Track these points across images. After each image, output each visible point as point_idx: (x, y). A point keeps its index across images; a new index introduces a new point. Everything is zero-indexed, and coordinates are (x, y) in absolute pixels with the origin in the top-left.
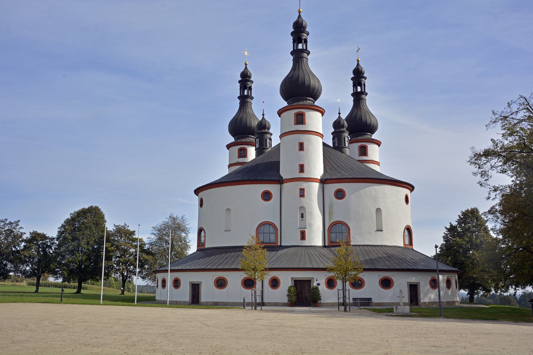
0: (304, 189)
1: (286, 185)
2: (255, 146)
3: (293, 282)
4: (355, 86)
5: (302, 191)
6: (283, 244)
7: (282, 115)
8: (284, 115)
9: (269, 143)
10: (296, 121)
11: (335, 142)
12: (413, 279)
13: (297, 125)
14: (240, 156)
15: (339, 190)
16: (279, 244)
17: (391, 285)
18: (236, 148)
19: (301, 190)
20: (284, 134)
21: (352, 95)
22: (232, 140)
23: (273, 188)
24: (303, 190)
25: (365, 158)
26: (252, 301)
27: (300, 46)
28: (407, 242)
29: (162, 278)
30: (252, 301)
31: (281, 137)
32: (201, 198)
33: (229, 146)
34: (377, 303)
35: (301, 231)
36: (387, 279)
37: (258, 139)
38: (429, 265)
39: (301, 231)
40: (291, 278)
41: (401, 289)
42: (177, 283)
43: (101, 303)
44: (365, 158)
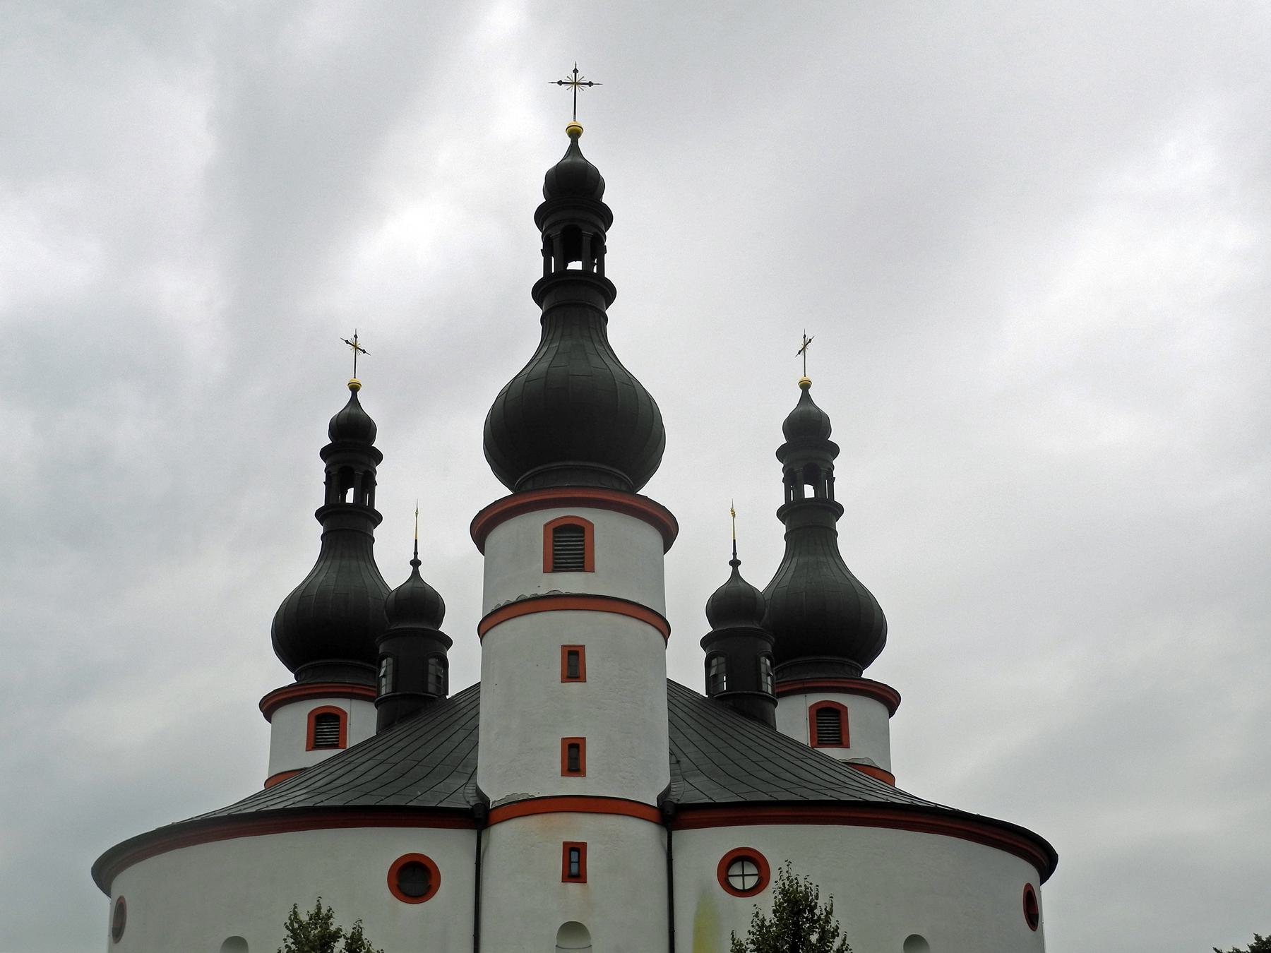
0: (585, 844)
1: (502, 834)
4: (792, 481)
5: (574, 856)
9: (438, 677)
11: (715, 676)
13: (554, 571)
14: (315, 743)
15: (736, 855)
18: (298, 716)
20: (500, 616)
24: (577, 850)
33: (272, 704)
37: (390, 660)
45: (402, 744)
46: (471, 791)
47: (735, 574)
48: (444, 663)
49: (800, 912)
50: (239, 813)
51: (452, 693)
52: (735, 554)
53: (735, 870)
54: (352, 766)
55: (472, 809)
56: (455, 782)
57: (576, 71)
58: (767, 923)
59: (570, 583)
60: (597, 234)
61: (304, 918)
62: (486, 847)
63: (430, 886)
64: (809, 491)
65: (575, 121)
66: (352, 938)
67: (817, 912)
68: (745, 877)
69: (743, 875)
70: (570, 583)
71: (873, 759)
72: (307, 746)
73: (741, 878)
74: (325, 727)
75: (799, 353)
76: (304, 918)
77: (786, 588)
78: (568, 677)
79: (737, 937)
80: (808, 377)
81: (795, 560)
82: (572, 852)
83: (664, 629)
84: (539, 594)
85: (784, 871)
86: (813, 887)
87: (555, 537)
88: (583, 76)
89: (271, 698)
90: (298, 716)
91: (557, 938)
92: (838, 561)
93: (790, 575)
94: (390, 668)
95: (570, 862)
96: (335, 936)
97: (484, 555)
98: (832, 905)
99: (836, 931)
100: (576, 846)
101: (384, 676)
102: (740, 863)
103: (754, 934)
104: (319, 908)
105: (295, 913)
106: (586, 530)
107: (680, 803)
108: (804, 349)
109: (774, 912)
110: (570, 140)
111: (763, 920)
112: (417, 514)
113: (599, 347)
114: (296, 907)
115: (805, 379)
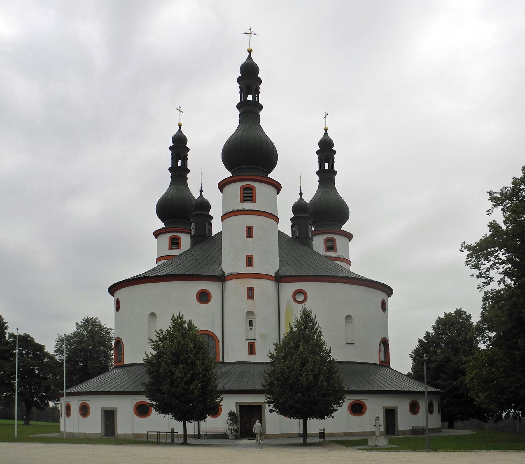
1: (230, 284)
2: (189, 233)
3: (238, 407)
4: (321, 162)
6: (226, 360)
7: (224, 190)
8: (227, 188)
9: (209, 229)
10: (242, 198)
12: (390, 402)
13: (244, 202)
14: (171, 247)
15: (298, 291)
16: (221, 360)
17: (363, 411)
18: (166, 238)
19: (250, 289)
20: (228, 215)
21: (318, 173)
22: (161, 225)
23: (213, 288)
25: (332, 254)
26: (175, 432)
27: (250, 98)
28: (383, 359)
29: (66, 403)
30: (175, 432)
31: (224, 217)
32: (118, 299)
33: (157, 234)
34: (346, 433)
35: (249, 343)
36: (357, 403)
38: (409, 386)
39: (249, 343)
40: (236, 403)
41: (377, 415)
42: (85, 410)
43: (16, 435)
44: (332, 254)
45: (199, 253)
46: (220, 270)
47: (301, 197)
48: (211, 225)
49: (307, 318)
50: (151, 275)
51: (213, 234)
52: (301, 191)
53: (298, 295)
54: (184, 260)
55: (220, 276)
56: (215, 266)
57: (250, 29)
58: (298, 320)
59: (248, 206)
60: (257, 87)
61: (176, 317)
62: (225, 286)
63: (209, 299)
64: (326, 166)
65: (250, 47)
66: (189, 323)
67: (312, 317)
68: (301, 298)
69: (300, 297)
70: (248, 206)
71: (344, 256)
72: (169, 248)
73: (299, 298)
74: (174, 242)
75: (324, 118)
76: (176, 317)
77: (318, 199)
78: (248, 236)
79: (290, 324)
80: (327, 127)
81: (321, 190)
82: (250, 290)
83: (277, 220)
84: (239, 209)
85: (303, 306)
86: (311, 311)
87: (243, 191)
88: (253, 31)
89: (156, 232)
90: (166, 238)
91: (246, 315)
92: (335, 190)
93: (320, 194)
94: (194, 227)
95: (249, 293)
96: (185, 322)
97: (222, 193)
98: (316, 316)
99: (317, 323)
100: (251, 288)
101: (192, 229)
102: (299, 294)
103: (295, 323)
104: (180, 315)
105: (173, 316)
106: (253, 189)
107: (281, 275)
108: (326, 116)
109: (300, 317)
110: (248, 53)
111: (298, 319)
112: (201, 175)
113: (257, 127)
114: (173, 314)
115: (326, 127)
